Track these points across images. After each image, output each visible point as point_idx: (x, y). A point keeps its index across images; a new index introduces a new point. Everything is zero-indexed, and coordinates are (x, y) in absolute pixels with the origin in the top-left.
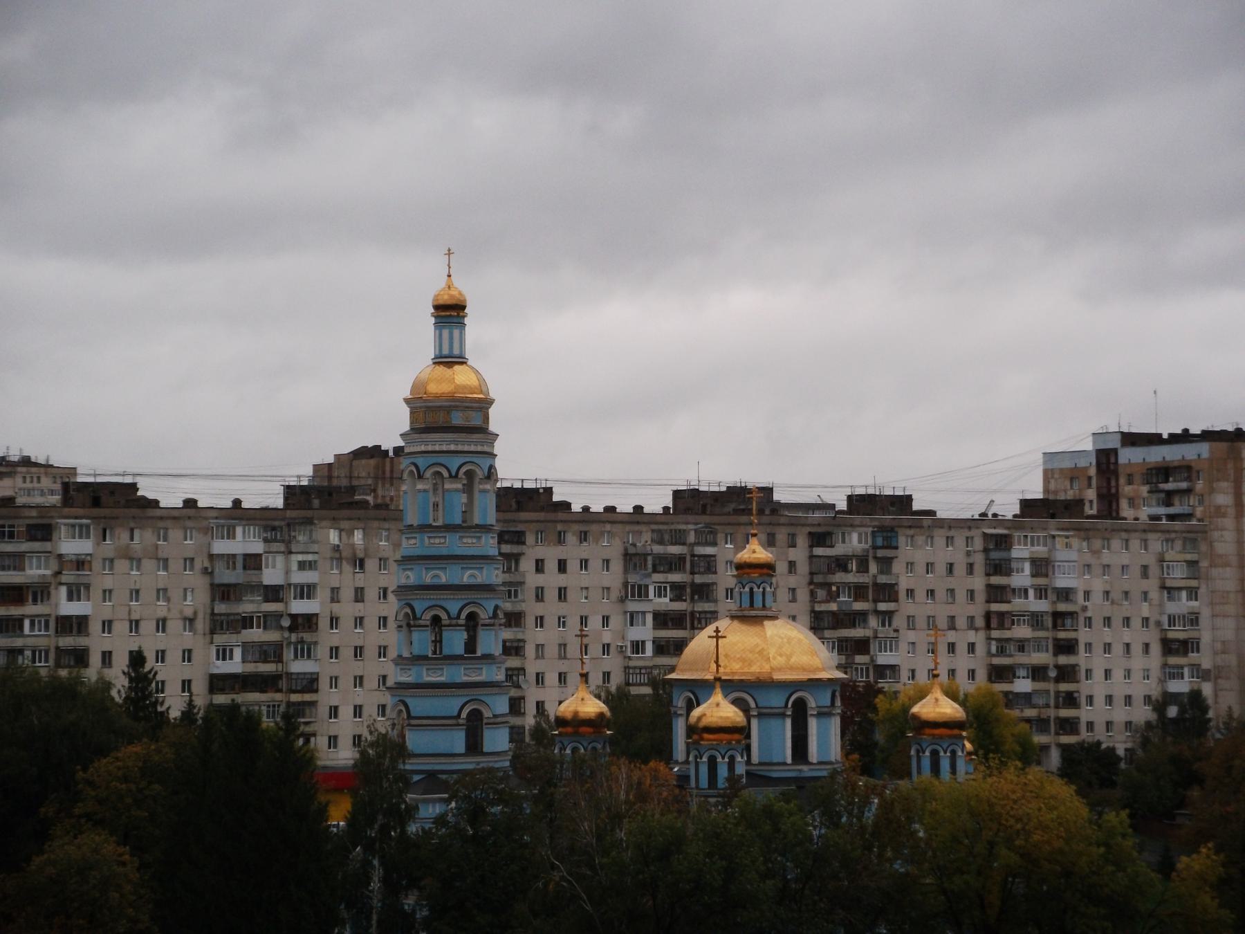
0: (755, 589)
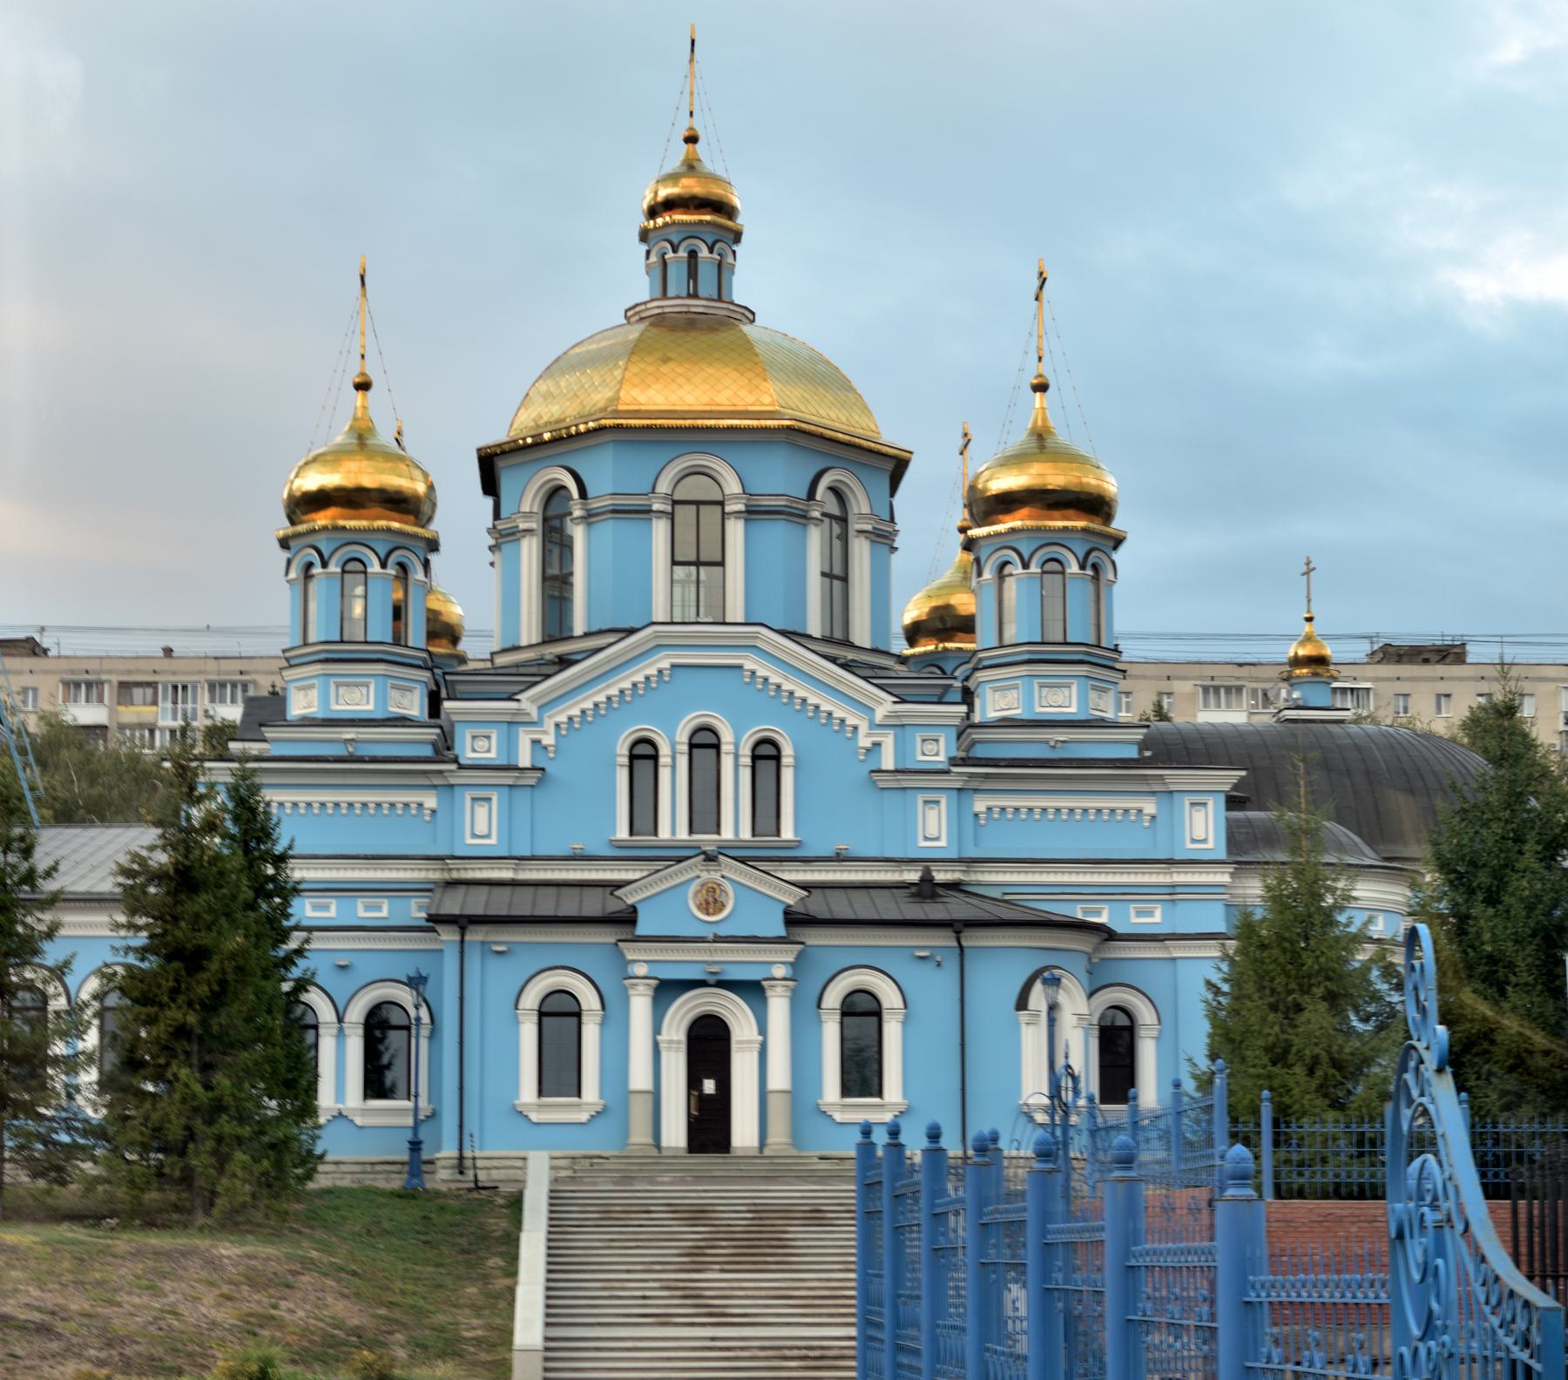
0: (704, 252)
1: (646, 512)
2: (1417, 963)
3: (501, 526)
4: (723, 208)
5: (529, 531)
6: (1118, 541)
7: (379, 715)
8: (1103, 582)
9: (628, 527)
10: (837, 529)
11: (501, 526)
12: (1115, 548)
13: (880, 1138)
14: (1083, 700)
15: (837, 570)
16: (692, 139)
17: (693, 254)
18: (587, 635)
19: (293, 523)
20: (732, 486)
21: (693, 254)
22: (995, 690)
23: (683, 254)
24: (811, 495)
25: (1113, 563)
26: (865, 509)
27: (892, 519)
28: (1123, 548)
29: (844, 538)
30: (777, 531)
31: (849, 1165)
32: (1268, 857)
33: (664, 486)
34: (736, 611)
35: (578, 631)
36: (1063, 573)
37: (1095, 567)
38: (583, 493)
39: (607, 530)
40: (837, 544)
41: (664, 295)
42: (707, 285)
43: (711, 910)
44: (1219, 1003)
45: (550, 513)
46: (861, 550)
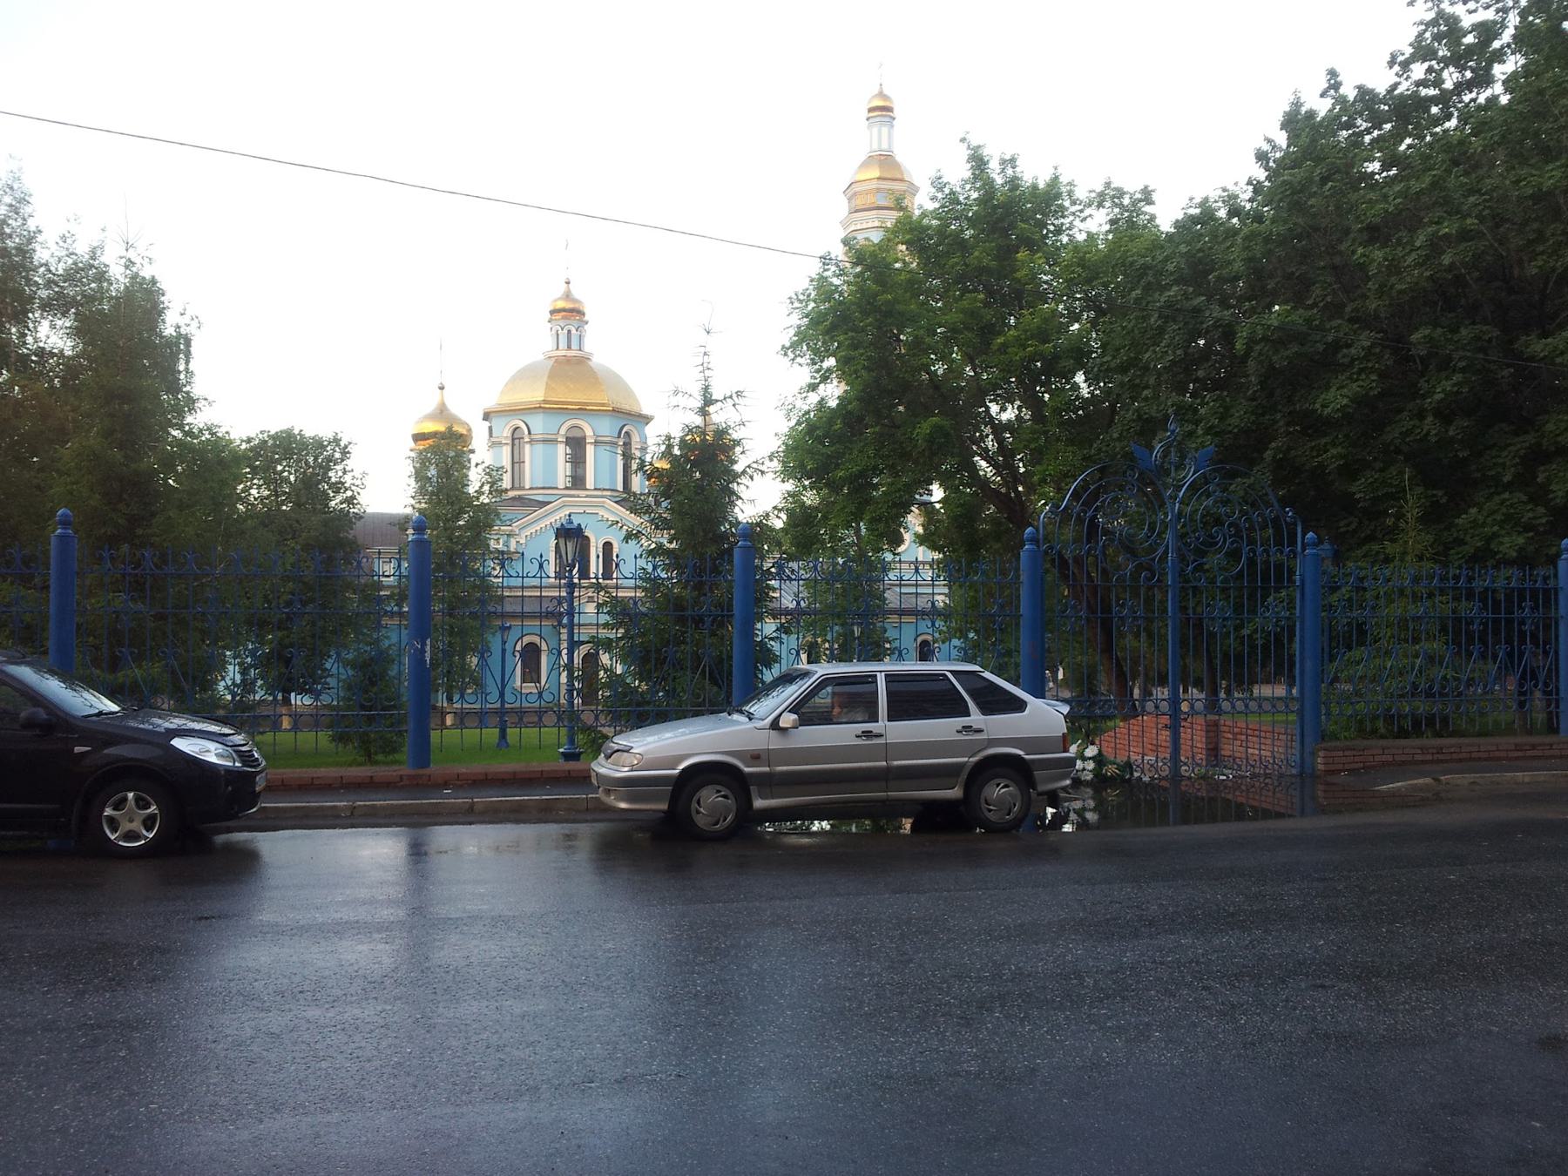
0: (574, 331)
1: (555, 441)
2: (1016, 411)
3: (492, 439)
4: (581, 313)
9: (549, 447)
11: (492, 439)
13: (456, 697)
16: (568, 283)
17: (569, 332)
18: (530, 489)
20: (589, 432)
21: (569, 332)
23: (565, 331)
32: (683, 738)
33: (563, 431)
34: (590, 483)
35: (527, 487)
38: (529, 433)
39: (539, 447)
41: (558, 348)
42: (574, 345)
43: (631, 601)
45: (515, 436)
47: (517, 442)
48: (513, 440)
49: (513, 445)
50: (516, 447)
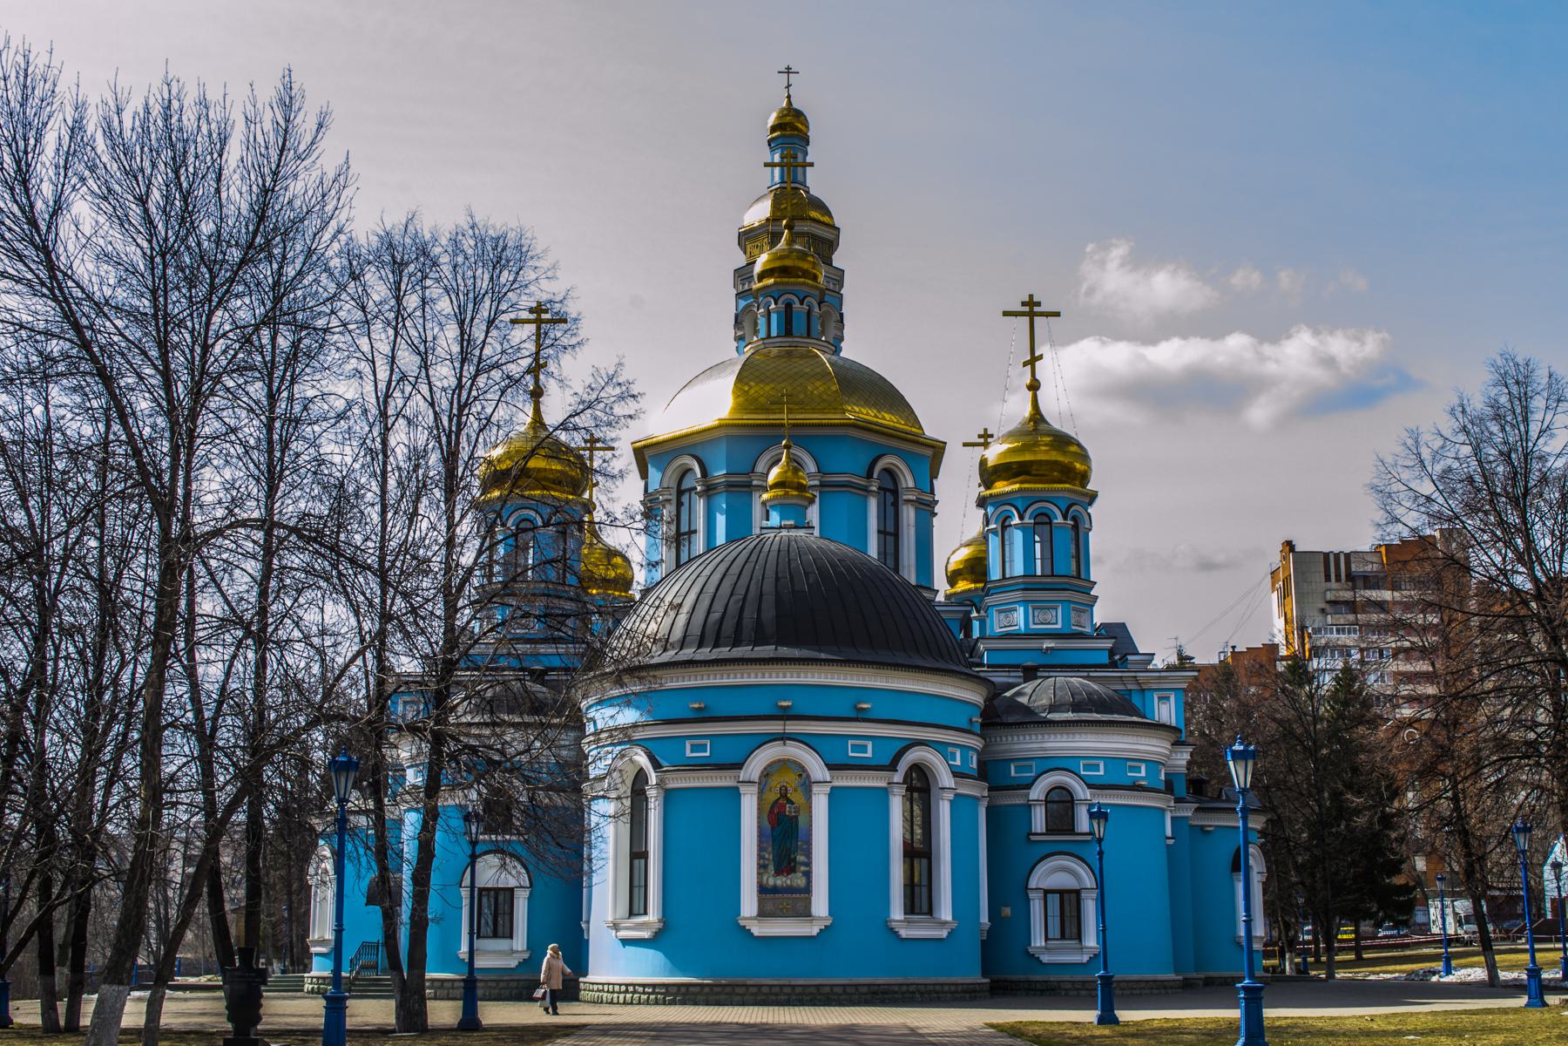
0: (797, 305)
5: (668, 501)
6: (1093, 497)
7: (1066, 631)
8: (1081, 531)
10: (890, 498)
12: (1090, 504)
14: (1066, 618)
15: (890, 528)
17: (789, 306)
19: (952, 586)
21: (789, 306)
22: (1000, 612)
23: (781, 305)
24: (869, 475)
25: (1089, 515)
26: (911, 484)
27: (932, 492)
28: (1098, 501)
29: (896, 505)
30: (843, 502)
31: (1118, 992)
36: (1050, 523)
37: (1074, 519)
40: (890, 510)
44: (251, 623)
46: (909, 515)
47: (685, 499)
48: (680, 493)
49: (679, 504)
50: (685, 510)
